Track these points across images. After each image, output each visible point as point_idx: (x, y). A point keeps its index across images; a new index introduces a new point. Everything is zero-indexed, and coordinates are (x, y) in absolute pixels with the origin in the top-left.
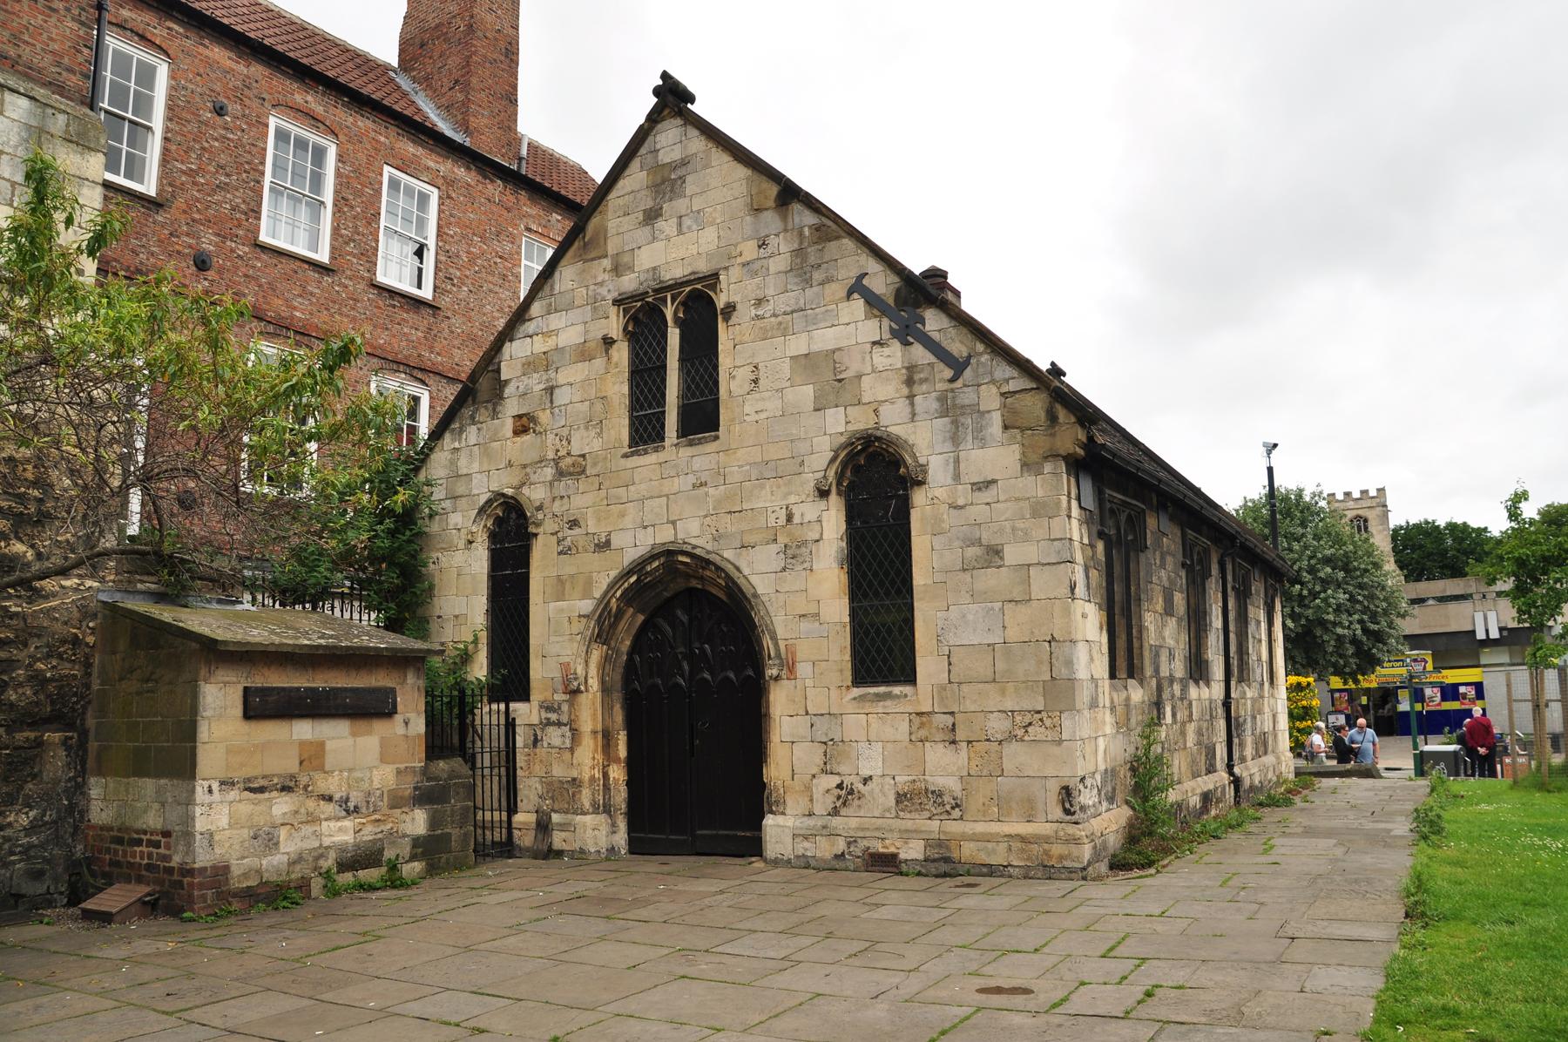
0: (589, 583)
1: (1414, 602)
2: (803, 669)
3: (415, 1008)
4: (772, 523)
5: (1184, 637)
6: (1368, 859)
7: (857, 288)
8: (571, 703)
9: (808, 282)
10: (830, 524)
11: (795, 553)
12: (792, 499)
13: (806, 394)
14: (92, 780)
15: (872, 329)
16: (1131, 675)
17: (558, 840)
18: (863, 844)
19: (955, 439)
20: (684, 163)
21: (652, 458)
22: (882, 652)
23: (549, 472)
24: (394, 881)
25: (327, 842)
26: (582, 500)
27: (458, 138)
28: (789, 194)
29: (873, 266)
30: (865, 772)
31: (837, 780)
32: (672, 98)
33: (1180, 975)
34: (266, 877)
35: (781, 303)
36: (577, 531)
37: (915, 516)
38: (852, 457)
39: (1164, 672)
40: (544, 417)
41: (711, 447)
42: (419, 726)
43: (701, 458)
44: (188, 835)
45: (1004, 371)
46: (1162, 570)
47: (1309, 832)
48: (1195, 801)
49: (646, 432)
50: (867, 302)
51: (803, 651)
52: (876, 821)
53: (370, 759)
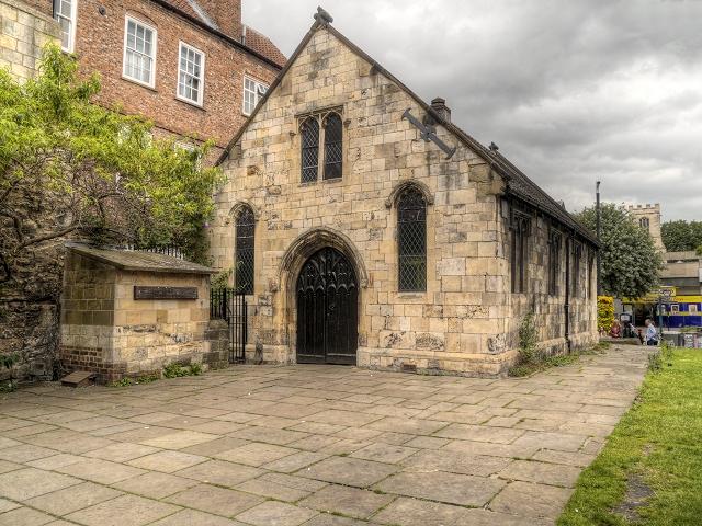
0: (282, 243)
1: (669, 262)
2: (377, 284)
3: (225, 418)
4: (365, 219)
5: (547, 275)
6: (624, 377)
7: (406, 115)
8: (273, 297)
9: (384, 111)
10: (390, 222)
11: (374, 233)
12: (375, 209)
13: (382, 162)
14: (63, 326)
15: (411, 134)
16: (521, 291)
17: (265, 356)
18: (401, 360)
19: (447, 185)
20: (328, 52)
21: (311, 188)
22: (411, 277)
23: (264, 193)
24: (195, 372)
25: (167, 354)
26: (279, 206)
27: (214, 27)
28: (377, 69)
29: (413, 105)
30: (403, 329)
31: (390, 332)
32: (323, 20)
33: (534, 415)
34: (142, 369)
35: (372, 120)
36: (276, 220)
37: (428, 218)
38: (401, 191)
39: (537, 291)
40: (262, 168)
41: (339, 184)
42: (207, 305)
43: (333, 189)
44: (109, 350)
45: (470, 155)
46: (538, 245)
47: (600, 365)
48: (549, 350)
49: (309, 176)
50: (411, 122)
51: (377, 276)
52: (406, 350)
53: (185, 321)
